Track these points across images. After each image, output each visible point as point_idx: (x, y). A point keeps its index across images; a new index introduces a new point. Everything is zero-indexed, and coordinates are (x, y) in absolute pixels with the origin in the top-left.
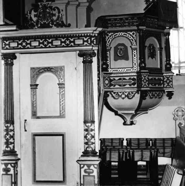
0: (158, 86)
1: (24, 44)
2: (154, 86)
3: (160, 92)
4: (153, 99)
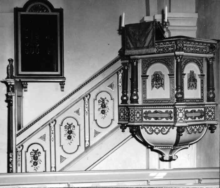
0: (199, 118)
1: (210, 114)
2: (194, 120)
3: (201, 126)
4: (193, 134)
